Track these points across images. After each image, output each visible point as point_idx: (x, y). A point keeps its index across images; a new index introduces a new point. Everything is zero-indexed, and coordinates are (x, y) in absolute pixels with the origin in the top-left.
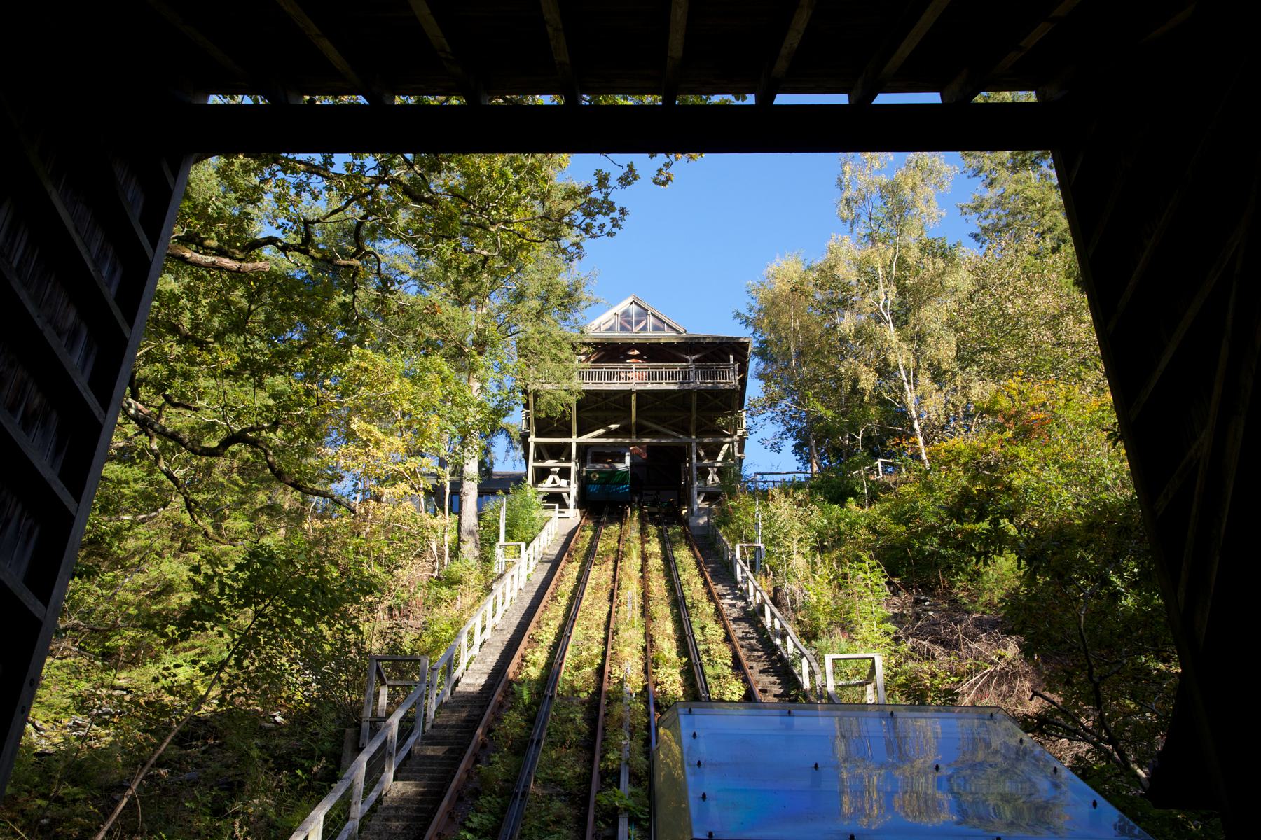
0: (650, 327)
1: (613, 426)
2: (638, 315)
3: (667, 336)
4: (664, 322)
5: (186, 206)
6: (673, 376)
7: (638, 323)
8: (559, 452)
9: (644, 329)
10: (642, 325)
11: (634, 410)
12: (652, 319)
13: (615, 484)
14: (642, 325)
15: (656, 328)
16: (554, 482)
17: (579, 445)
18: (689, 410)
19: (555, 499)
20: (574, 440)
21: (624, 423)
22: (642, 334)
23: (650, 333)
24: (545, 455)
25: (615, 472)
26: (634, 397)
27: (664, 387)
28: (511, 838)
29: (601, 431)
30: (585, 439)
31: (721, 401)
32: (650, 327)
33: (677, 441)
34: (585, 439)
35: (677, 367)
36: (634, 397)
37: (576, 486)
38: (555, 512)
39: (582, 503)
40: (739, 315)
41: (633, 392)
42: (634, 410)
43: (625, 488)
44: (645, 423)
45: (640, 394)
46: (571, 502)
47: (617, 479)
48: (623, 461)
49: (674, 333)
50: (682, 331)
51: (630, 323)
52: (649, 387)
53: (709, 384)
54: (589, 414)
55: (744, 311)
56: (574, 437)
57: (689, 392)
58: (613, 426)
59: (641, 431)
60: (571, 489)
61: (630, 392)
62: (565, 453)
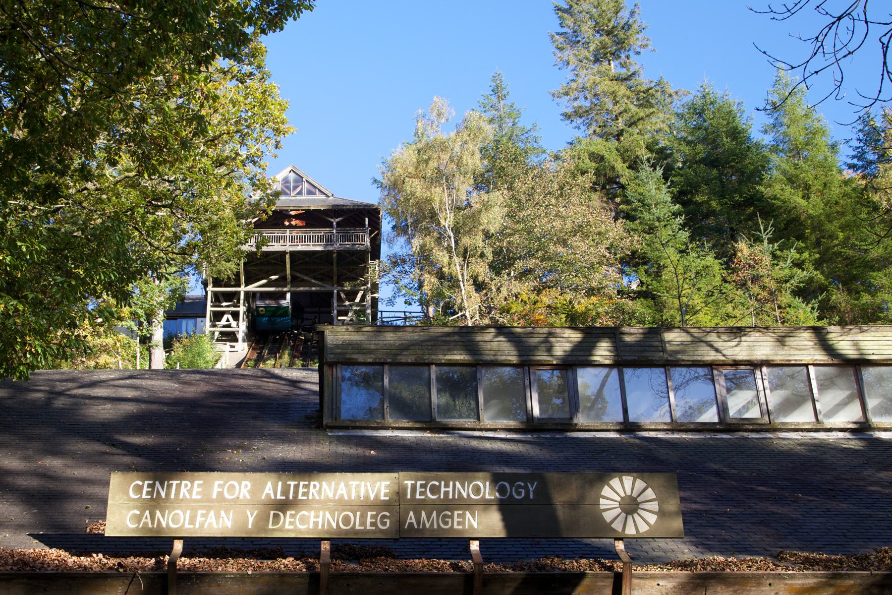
0: (305, 191)
1: (273, 277)
2: (296, 181)
3: (317, 202)
4: (316, 187)
5: (9, 402)
6: (320, 239)
7: (295, 188)
8: (232, 297)
9: (300, 193)
10: (298, 190)
11: (288, 266)
12: (306, 185)
13: (278, 316)
14: (298, 190)
15: (310, 193)
16: (228, 320)
17: (247, 294)
18: (332, 264)
19: (230, 337)
20: (242, 289)
21: (282, 274)
22: (299, 197)
23: (304, 197)
24: (221, 299)
25: (280, 307)
26: (288, 256)
27: (312, 248)
28: (889, 343)
29: (264, 281)
30: (252, 288)
31: (357, 257)
32: (305, 191)
33: (323, 289)
34: (252, 288)
35: (322, 232)
36: (288, 256)
37: (245, 323)
38: (226, 347)
39: (249, 337)
40: (375, 181)
41: (287, 253)
42: (288, 266)
43: (287, 320)
44: (298, 275)
45: (292, 254)
46: (240, 336)
47: (280, 312)
48: (285, 299)
49: (324, 197)
50: (330, 195)
51: (288, 187)
52: (299, 248)
53: (348, 245)
54: (255, 268)
55: (379, 178)
56: (243, 286)
57: (331, 252)
58: (273, 277)
59: (295, 280)
60: (241, 328)
61: (285, 253)
62: (236, 297)
